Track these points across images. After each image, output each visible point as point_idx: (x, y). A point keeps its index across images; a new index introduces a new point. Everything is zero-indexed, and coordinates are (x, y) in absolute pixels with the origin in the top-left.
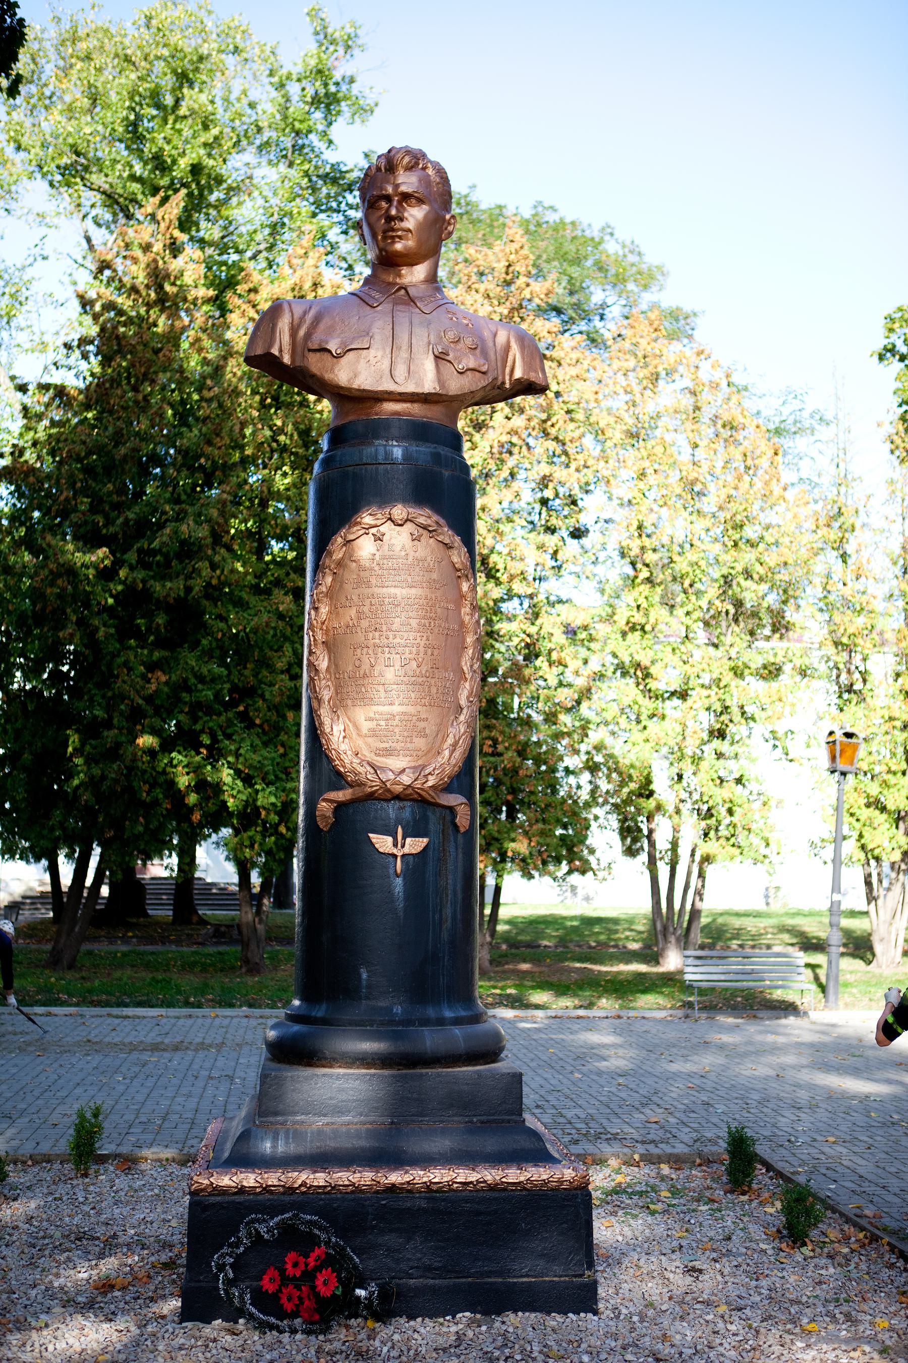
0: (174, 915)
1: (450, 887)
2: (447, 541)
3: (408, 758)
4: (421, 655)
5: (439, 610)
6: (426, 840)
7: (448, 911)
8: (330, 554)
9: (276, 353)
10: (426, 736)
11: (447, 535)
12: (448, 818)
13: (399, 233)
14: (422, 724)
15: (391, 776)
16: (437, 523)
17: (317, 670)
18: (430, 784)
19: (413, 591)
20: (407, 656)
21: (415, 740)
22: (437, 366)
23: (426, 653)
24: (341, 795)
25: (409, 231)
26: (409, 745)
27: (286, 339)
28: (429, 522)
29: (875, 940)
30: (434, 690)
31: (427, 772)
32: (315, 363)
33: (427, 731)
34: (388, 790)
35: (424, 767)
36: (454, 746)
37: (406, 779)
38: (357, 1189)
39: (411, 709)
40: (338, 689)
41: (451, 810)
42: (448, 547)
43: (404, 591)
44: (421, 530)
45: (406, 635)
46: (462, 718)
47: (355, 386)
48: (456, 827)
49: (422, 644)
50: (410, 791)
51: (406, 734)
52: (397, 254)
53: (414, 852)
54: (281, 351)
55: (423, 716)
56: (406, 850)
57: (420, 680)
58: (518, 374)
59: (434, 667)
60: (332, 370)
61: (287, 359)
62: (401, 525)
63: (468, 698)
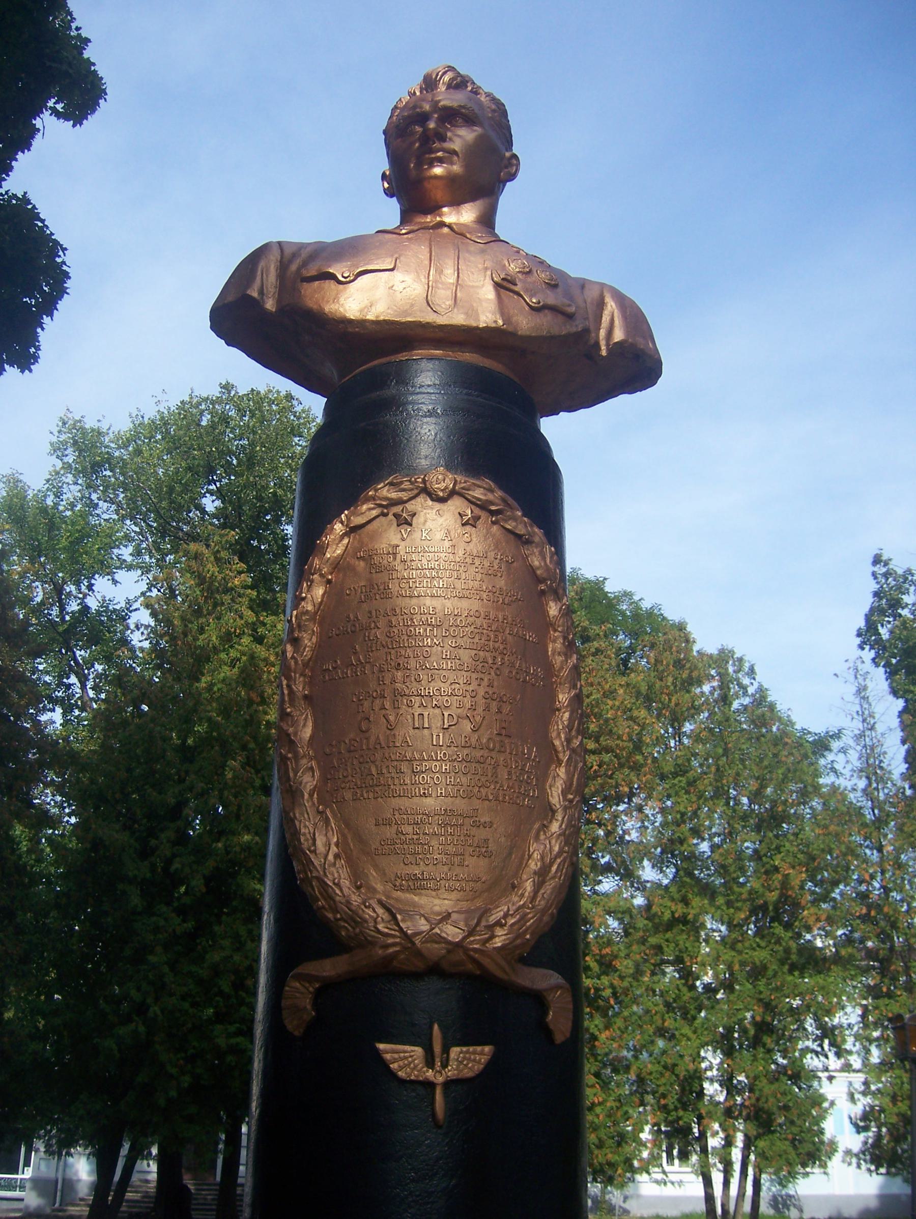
0: (93, 1200)
2: (521, 530)
3: (454, 895)
4: (480, 710)
5: (510, 638)
7: (416, 899)
8: (323, 550)
9: (255, 294)
10: (488, 855)
11: (520, 523)
13: (440, 154)
14: (482, 833)
15: (423, 926)
16: (504, 500)
17: (292, 742)
18: (498, 942)
19: (465, 604)
20: (454, 711)
21: (470, 861)
22: (499, 296)
23: (487, 708)
24: (329, 968)
25: (455, 153)
26: (457, 870)
27: (272, 278)
28: (490, 497)
30: (503, 774)
31: (493, 919)
33: (492, 846)
34: (419, 954)
35: (486, 912)
36: (542, 874)
37: (452, 932)
39: (461, 805)
40: (328, 775)
41: (539, 1000)
42: (522, 540)
43: (448, 603)
44: (477, 511)
45: (452, 676)
46: (555, 827)
47: (370, 317)
49: (481, 692)
50: (460, 955)
51: (451, 849)
53: (467, 1074)
54: (261, 292)
55: (485, 818)
56: (451, 1072)
57: (478, 754)
58: (619, 335)
59: (504, 733)
60: (336, 299)
61: (270, 305)
62: (442, 500)
63: (564, 793)
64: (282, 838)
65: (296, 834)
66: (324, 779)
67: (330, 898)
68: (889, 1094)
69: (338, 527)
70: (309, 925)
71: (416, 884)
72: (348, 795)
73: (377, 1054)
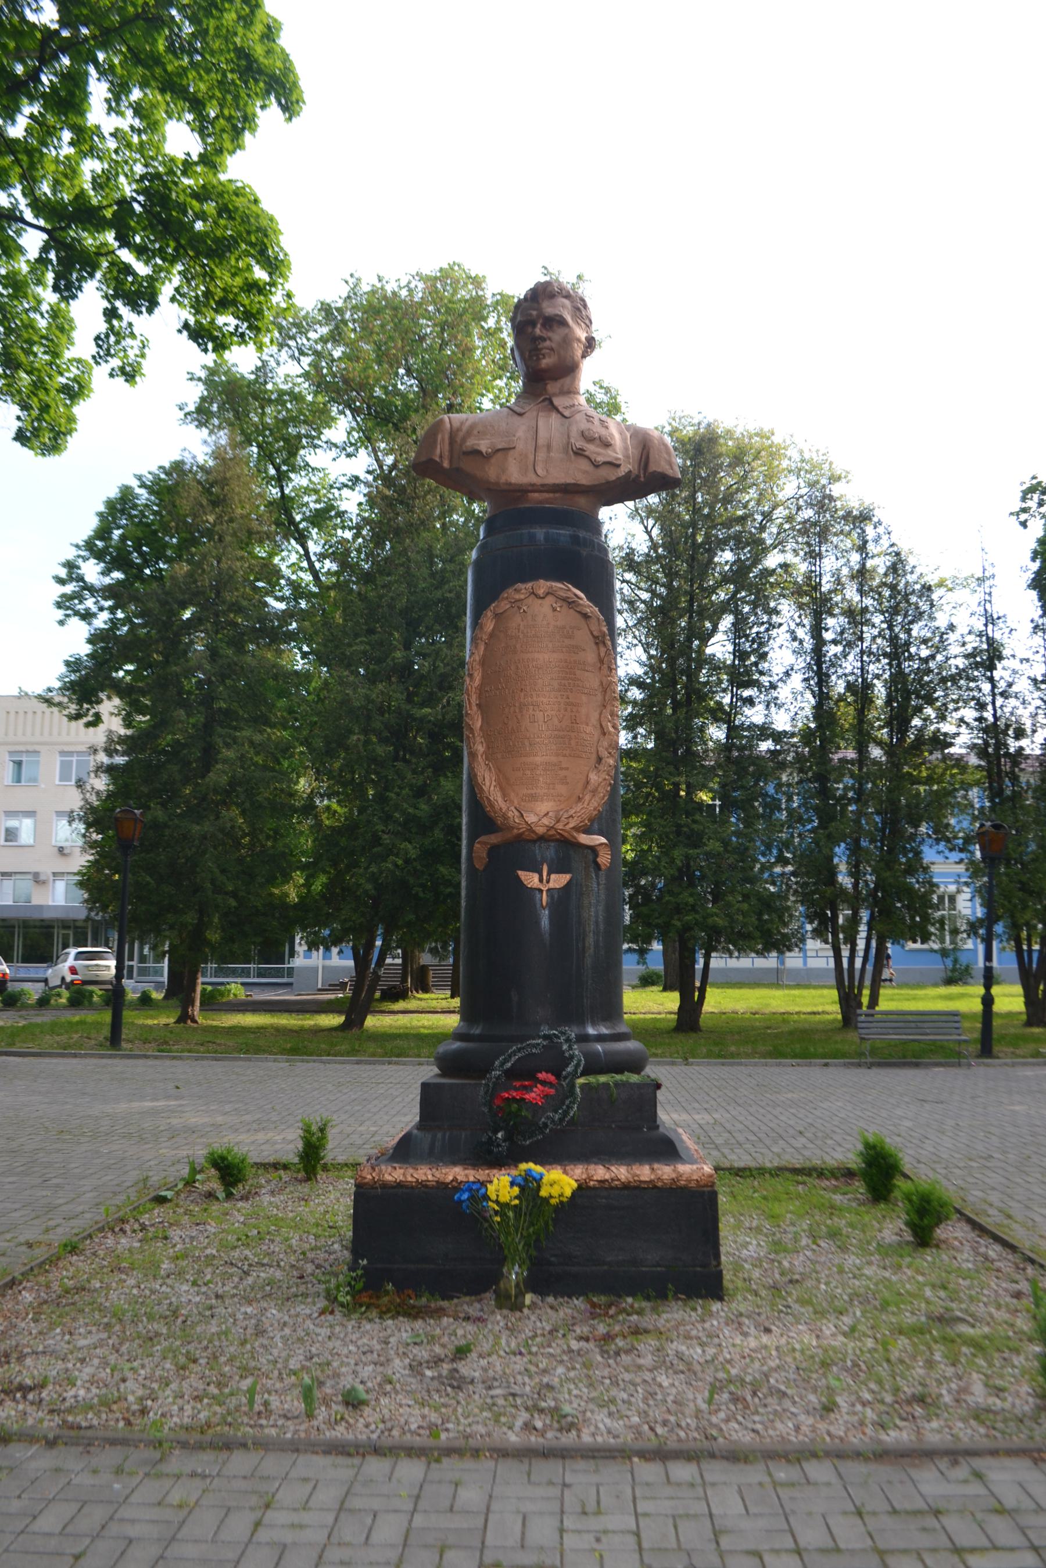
1: (593, 919)
6: (568, 877)
7: (590, 940)
12: (591, 857)
18: (571, 825)
24: (494, 839)
29: (13, 435)
32: (468, 465)
34: (534, 832)
38: (422, 1185)
41: (593, 850)
48: (598, 866)
52: (544, 371)
54: (441, 457)
56: (551, 885)
61: (446, 464)
64: (469, 775)
65: (476, 775)
66: (488, 748)
67: (492, 806)
68: (325, 1168)
69: (489, 614)
70: (484, 821)
71: (533, 798)
72: (499, 756)
73: (518, 877)
